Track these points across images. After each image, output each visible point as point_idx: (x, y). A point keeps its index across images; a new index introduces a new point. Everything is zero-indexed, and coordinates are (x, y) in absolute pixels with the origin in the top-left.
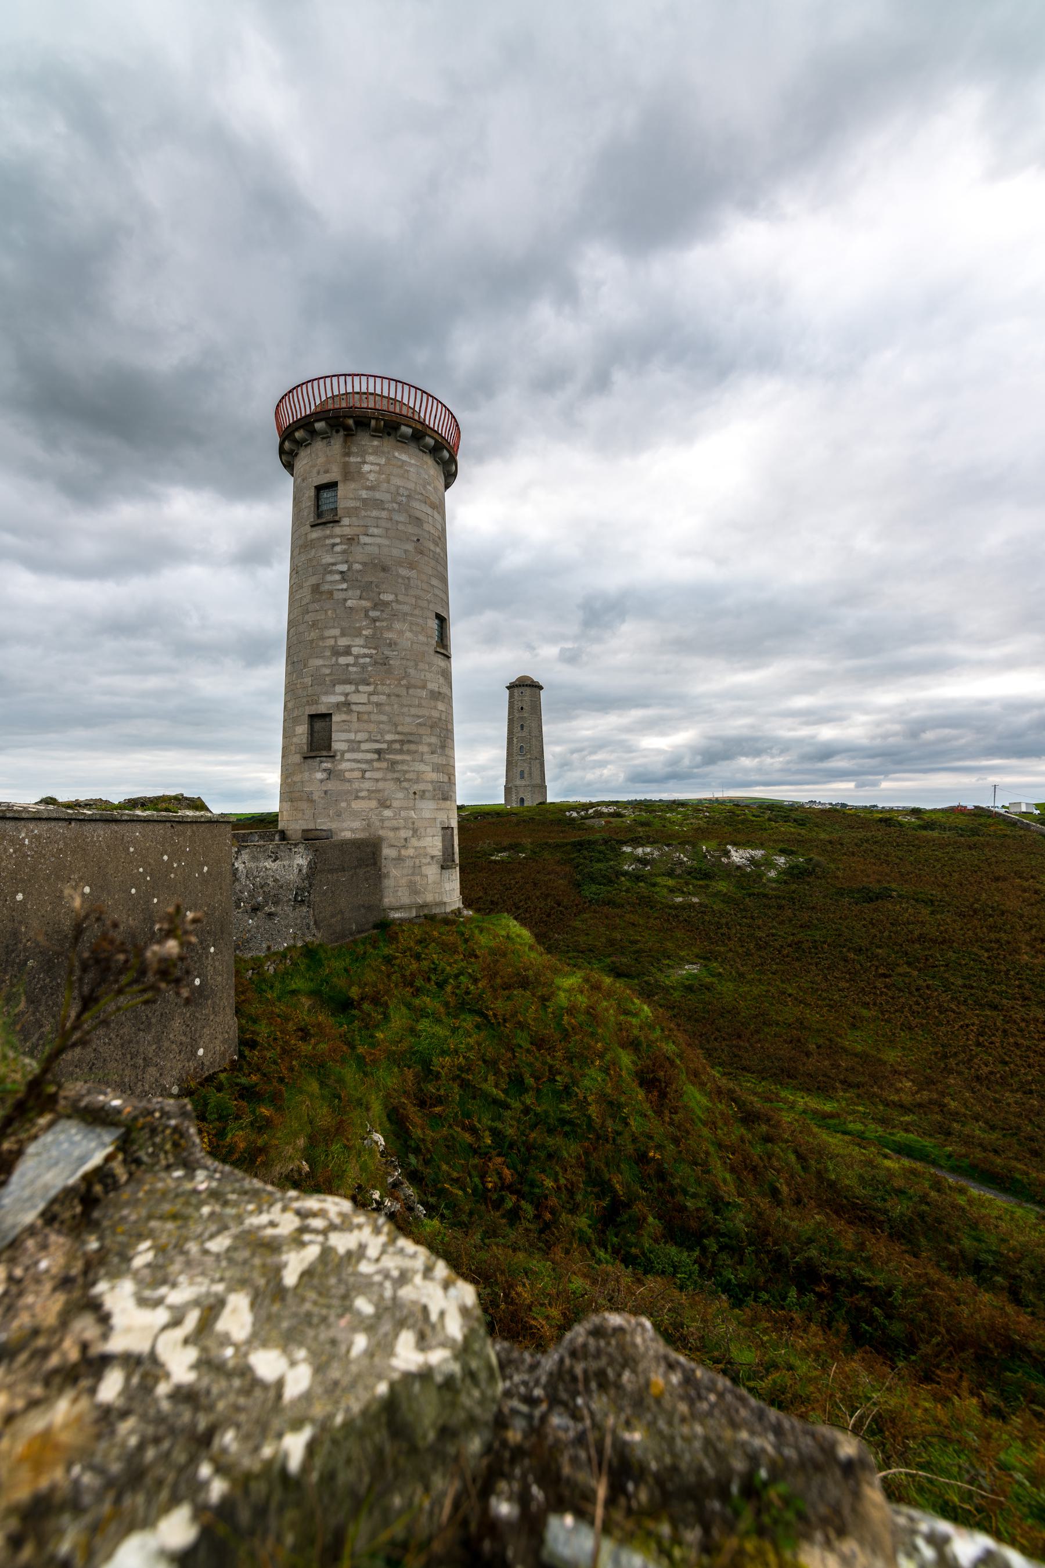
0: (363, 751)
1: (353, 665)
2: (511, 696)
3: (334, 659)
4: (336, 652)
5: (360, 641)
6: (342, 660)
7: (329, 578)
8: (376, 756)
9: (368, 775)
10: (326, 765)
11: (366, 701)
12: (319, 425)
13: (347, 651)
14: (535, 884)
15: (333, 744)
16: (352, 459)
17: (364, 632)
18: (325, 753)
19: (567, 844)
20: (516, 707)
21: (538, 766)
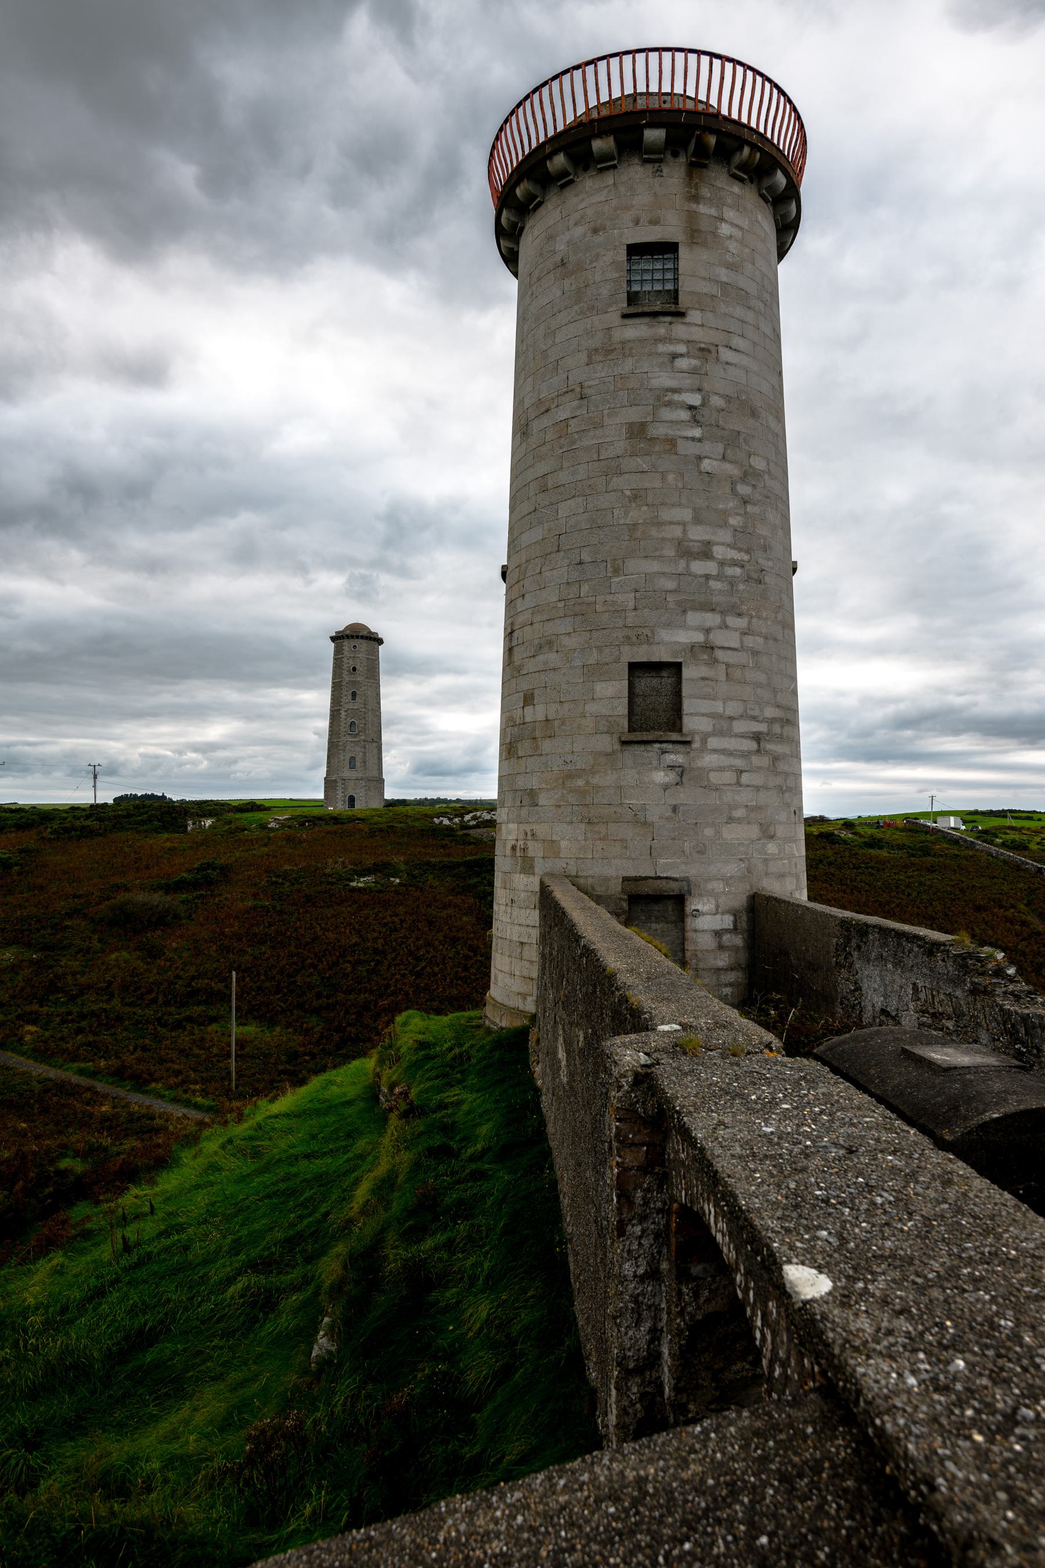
0: (736, 736)
1: (718, 577)
2: (338, 651)
3: (682, 564)
4: (686, 552)
5: (725, 536)
6: (699, 567)
7: (666, 414)
8: (753, 745)
9: (745, 778)
10: (675, 758)
11: (737, 645)
12: (654, 135)
13: (705, 553)
14: (431, 923)
15: (686, 720)
16: (703, 209)
17: (732, 521)
18: (675, 736)
19: (458, 865)
20: (345, 666)
21: (375, 751)
